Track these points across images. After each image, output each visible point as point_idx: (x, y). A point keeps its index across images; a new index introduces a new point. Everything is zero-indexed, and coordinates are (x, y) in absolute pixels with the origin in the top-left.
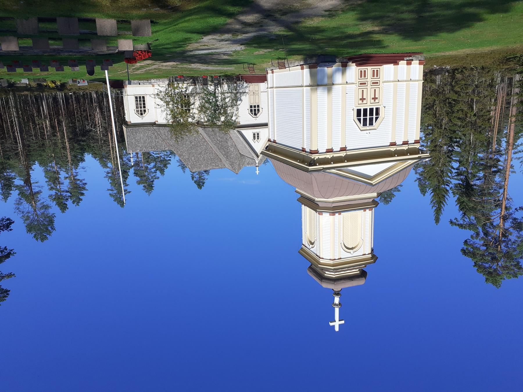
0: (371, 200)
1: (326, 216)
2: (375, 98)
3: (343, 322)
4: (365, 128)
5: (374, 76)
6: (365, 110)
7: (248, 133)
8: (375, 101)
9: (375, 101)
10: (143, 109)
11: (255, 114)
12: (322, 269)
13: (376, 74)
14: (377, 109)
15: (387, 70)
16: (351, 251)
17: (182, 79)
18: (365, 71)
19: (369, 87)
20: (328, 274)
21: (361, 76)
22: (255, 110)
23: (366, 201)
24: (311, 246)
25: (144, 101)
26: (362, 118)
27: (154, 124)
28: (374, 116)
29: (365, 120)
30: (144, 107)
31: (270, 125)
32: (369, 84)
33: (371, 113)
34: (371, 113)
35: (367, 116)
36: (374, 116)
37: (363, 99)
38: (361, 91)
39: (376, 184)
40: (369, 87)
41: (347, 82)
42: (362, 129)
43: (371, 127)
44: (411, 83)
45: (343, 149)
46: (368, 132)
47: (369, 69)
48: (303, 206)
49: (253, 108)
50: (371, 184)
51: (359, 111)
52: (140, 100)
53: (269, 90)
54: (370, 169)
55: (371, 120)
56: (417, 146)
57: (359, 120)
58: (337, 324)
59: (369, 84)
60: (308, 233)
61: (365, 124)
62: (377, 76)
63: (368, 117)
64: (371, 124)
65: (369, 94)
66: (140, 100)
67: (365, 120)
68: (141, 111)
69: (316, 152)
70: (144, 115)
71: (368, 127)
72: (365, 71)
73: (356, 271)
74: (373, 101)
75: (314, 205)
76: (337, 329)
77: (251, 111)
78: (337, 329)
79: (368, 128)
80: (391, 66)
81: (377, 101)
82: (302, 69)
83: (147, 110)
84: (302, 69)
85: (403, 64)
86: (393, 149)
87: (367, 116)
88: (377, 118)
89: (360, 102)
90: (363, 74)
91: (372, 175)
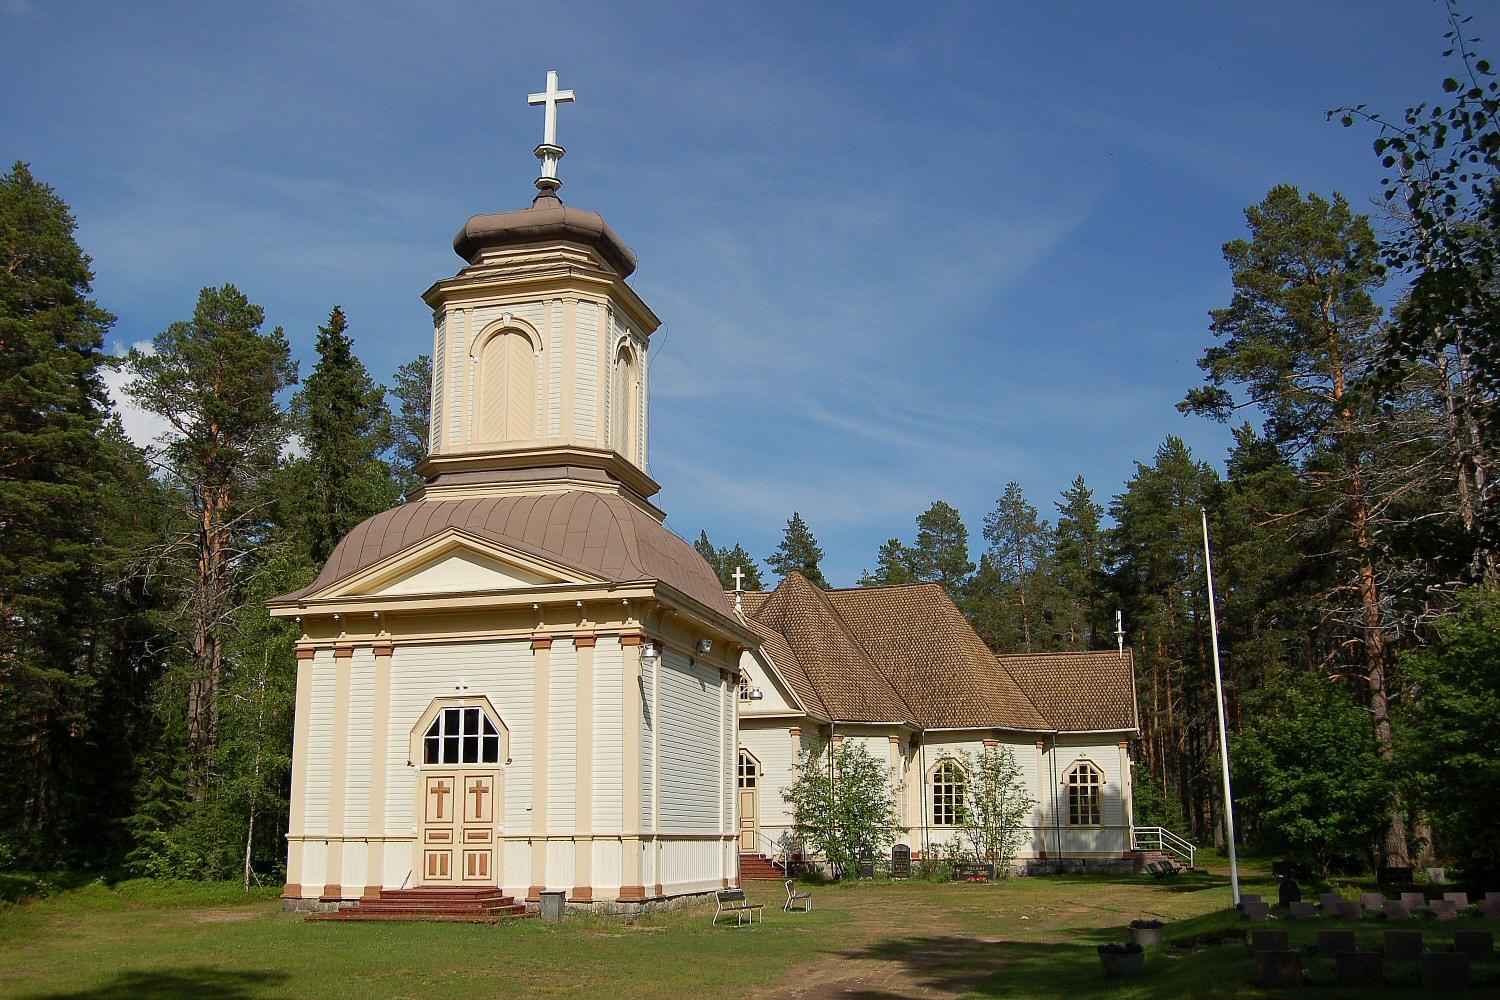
0: (443, 479)
1: (592, 436)
2: (441, 791)
3: (533, 98)
4: (471, 704)
5: (444, 859)
6: (470, 756)
7: (773, 703)
8: (479, 783)
9: (479, 783)
10: (943, 784)
11: (1083, 769)
12: (598, 271)
13: (436, 863)
14: (431, 756)
15: (400, 871)
16: (507, 323)
17: (960, 869)
18: (472, 873)
19: (458, 826)
20: (580, 255)
21: (483, 859)
22: (1084, 780)
23: (453, 479)
24: (627, 344)
25: (938, 810)
26: (481, 736)
27: (1047, 741)
28: (442, 737)
29: (471, 726)
30: (937, 789)
31: (735, 723)
32: (458, 836)
33: (451, 746)
34: (451, 746)
35: (462, 737)
36: (442, 737)
37: (479, 791)
38: (447, 816)
39: (442, 531)
40: (458, 826)
41: (530, 842)
42: (483, 702)
43: (452, 705)
44: (326, 833)
45: (545, 643)
46: (462, 693)
47: (457, 877)
48: (643, 470)
49: (745, 777)
50: (458, 531)
51: (491, 754)
52: (1085, 811)
53: (733, 832)
54: (457, 578)
55: (452, 727)
56: (305, 641)
57: (489, 728)
58: (552, 92)
59: (458, 836)
60: (633, 384)
61: (472, 715)
62: (433, 859)
63: (461, 736)
64: (452, 716)
65: (459, 807)
66: (1085, 811)
67: (471, 726)
68: (1084, 780)
69: (624, 639)
70: (1077, 766)
71: (462, 706)
72: (472, 873)
73: (494, 257)
74: (448, 783)
75: (617, 469)
76: (552, 78)
77: (751, 771)
78: (552, 78)
79: (462, 702)
80: (391, 884)
81: (434, 783)
82: (659, 888)
83: (1067, 779)
84: (659, 888)
85: (353, 888)
86: (385, 637)
87: (462, 737)
88: (435, 730)
89: (486, 782)
90: (478, 863)
91: (455, 559)
